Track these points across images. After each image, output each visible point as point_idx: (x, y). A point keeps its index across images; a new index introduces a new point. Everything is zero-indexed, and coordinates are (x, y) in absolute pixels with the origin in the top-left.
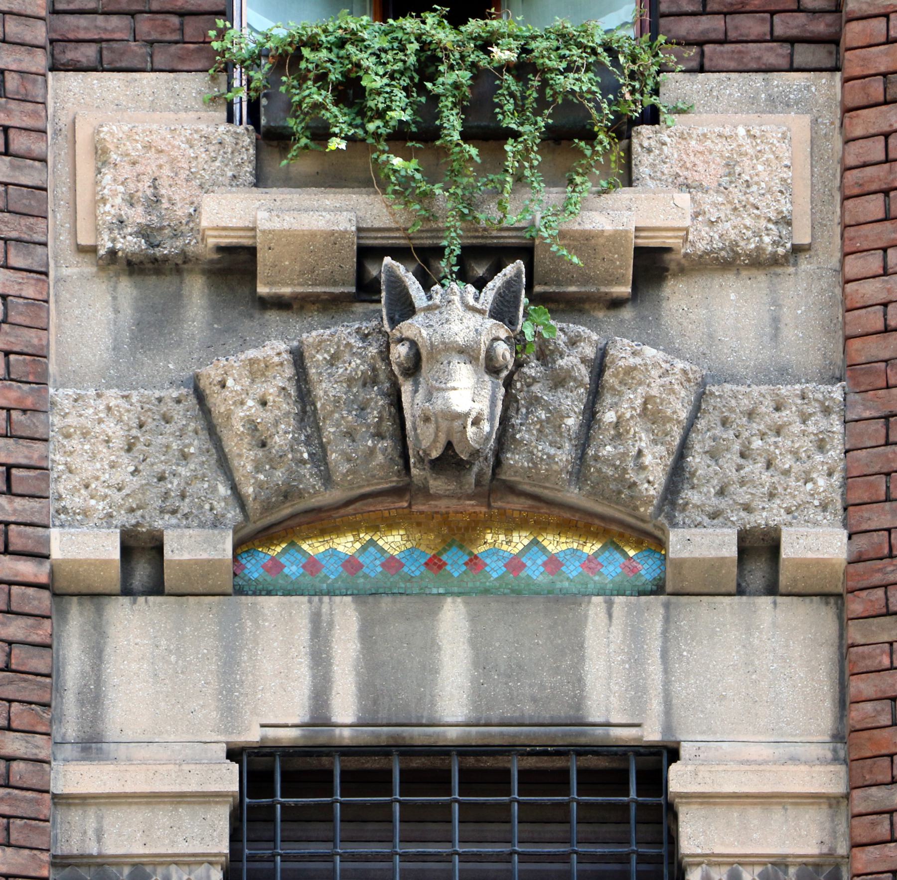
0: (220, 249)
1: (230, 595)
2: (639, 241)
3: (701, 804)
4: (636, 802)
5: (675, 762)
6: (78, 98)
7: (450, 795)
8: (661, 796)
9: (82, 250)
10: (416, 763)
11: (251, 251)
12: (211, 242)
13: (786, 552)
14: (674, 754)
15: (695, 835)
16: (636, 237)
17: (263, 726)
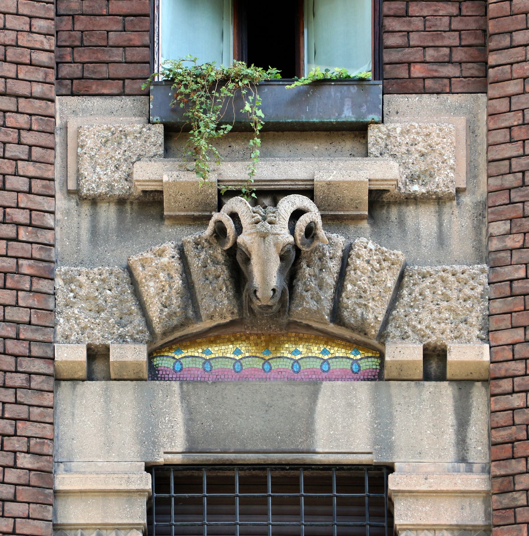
0: (144, 192)
1: (146, 380)
2: (371, 186)
3: (93, 496)
4: (369, 496)
5: (392, 473)
6: (67, 109)
7: (299, 493)
8: (383, 493)
9: (69, 192)
10: (344, 474)
11: (161, 192)
12: (140, 188)
13: (451, 358)
14: (390, 469)
15: (403, 515)
16: (218, 185)
17: (165, 453)
